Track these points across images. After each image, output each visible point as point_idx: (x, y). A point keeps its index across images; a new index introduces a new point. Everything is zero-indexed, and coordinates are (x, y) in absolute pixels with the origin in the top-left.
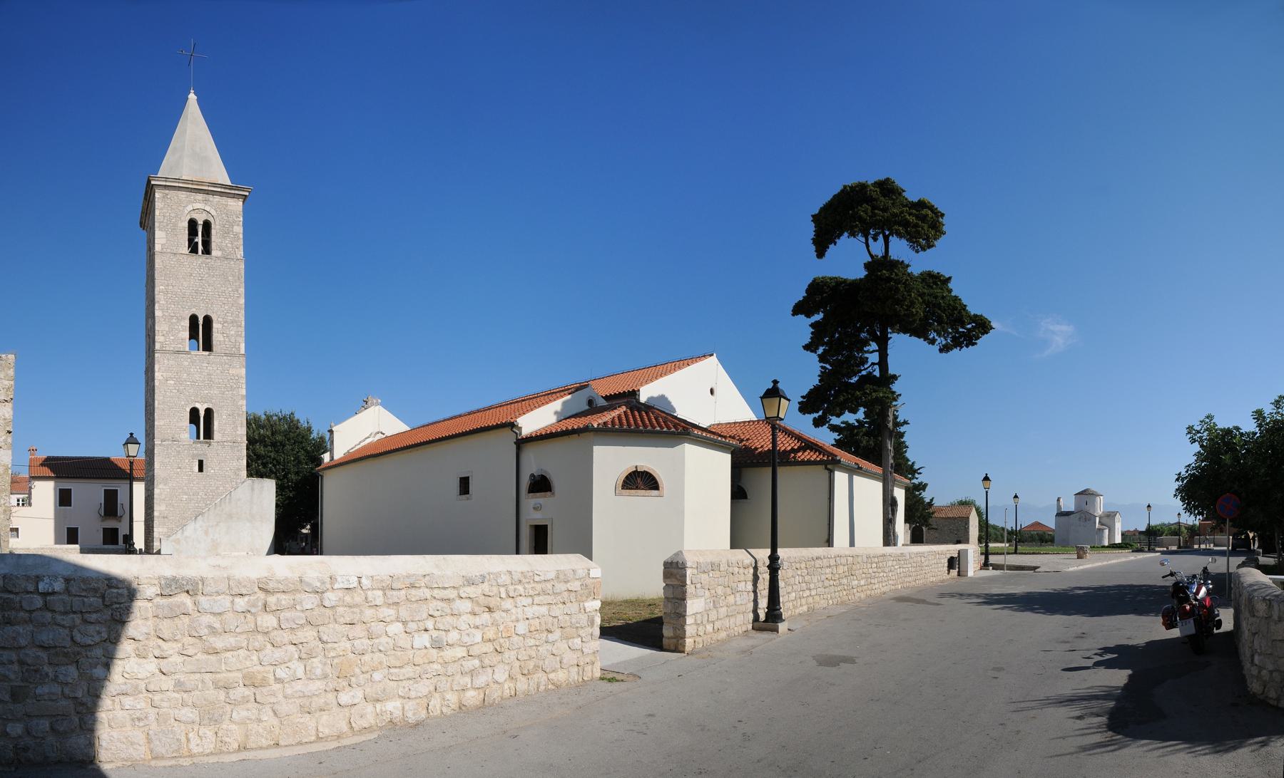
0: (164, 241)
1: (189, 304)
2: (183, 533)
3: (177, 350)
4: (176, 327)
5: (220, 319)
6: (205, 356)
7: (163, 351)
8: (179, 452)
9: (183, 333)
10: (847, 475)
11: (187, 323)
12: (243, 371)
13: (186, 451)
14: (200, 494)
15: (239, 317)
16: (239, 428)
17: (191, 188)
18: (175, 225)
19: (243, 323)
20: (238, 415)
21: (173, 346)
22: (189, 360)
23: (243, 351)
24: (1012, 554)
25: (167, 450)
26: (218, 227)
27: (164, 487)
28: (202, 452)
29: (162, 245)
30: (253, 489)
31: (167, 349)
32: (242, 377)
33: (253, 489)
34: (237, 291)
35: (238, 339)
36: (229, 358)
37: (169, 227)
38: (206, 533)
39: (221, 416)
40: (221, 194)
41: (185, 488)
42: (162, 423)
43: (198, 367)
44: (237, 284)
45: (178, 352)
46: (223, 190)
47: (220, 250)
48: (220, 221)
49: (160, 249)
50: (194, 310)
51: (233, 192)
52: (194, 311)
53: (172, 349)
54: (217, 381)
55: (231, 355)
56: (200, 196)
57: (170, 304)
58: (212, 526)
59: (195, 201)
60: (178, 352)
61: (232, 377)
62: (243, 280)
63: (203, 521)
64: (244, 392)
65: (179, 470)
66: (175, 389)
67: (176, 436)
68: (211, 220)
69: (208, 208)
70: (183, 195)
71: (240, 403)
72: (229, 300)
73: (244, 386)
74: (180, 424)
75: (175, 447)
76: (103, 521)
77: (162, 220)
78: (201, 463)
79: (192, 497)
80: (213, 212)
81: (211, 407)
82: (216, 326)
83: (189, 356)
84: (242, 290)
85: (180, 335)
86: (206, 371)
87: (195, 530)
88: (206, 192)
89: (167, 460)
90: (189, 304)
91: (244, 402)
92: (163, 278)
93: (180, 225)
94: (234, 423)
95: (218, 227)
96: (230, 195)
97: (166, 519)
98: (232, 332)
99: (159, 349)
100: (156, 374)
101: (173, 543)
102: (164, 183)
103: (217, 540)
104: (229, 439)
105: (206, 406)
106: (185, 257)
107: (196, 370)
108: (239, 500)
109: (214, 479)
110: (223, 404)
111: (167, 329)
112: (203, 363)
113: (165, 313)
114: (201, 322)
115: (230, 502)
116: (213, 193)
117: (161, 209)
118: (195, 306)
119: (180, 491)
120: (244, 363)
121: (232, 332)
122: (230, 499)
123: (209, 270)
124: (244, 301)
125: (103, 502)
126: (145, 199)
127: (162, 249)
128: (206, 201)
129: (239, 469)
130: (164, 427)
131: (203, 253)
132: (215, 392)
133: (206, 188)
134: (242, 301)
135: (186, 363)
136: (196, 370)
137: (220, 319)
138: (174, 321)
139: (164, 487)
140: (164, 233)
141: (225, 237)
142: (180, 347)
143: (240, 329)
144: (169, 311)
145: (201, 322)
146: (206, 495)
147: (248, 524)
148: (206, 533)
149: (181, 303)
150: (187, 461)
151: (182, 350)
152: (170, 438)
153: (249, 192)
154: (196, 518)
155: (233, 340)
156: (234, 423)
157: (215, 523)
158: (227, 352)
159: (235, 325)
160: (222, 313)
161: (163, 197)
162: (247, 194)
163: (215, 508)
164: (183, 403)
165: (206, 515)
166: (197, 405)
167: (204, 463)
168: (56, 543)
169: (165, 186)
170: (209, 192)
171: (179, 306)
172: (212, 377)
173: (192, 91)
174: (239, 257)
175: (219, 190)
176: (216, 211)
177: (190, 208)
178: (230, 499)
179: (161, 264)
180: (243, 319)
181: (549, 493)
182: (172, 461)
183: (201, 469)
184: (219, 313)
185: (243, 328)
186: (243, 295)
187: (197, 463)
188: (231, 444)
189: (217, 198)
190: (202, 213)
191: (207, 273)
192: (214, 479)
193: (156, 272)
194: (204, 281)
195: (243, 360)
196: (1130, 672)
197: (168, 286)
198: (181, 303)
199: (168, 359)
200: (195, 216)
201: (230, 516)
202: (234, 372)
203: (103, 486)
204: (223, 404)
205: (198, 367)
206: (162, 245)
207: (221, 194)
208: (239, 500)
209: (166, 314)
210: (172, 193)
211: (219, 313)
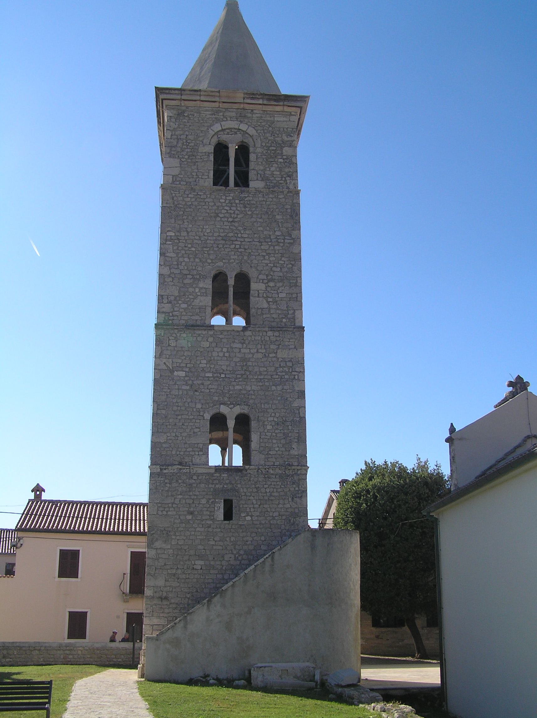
2: (185, 627)
4: (191, 290)
5: (261, 277)
9: (202, 298)
10: (416, 621)
11: (208, 284)
13: (202, 485)
14: (227, 557)
21: (186, 318)
22: (211, 339)
24: (256, 180)
27: (164, 546)
28: (230, 486)
29: (173, 176)
37: (184, 153)
39: (264, 425)
50: (220, 264)
65: (189, 517)
66: (187, 384)
68: (250, 142)
69: (243, 127)
72: (277, 248)
76: (126, 601)
79: (212, 563)
80: (251, 131)
89: (169, 500)
95: (259, 150)
97: (165, 602)
98: (281, 295)
101: (168, 646)
105: (237, 410)
107: (221, 354)
111: (176, 294)
112: (234, 342)
113: (173, 270)
114: (231, 282)
121: (281, 295)
123: (245, 207)
125: (128, 571)
126: (159, 123)
131: (236, 185)
132: (254, 387)
135: (206, 344)
137: (261, 277)
139: (164, 546)
145: (231, 282)
150: (204, 501)
158: (274, 324)
164: (199, 406)
166: (224, 409)
168: (69, 637)
172: (250, 363)
176: (257, 131)
177: (217, 127)
181: (140, 596)
182: (177, 501)
183: (228, 515)
184: (260, 268)
190: (236, 133)
191: (241, 212)
200: (224, 138)
202: (285, 356)
203: (128, 547)
204: (267, 406)
205: (225, 350)
206: (173, 176)
211: (260, 268)
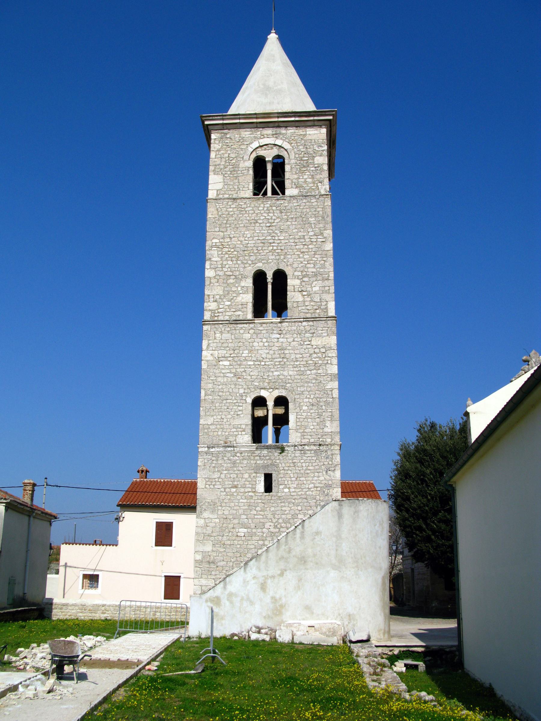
0: (220, 186)
1: (253, 258)
2: (225, 587)
3: (234, 318)
5: (296, 273)
6: (276, 323)
7: (214, 322)
8: (234, 463)
9: (244, 296)
11: (249, 283)
12: (333, 340)
14: (267, 525)
15: (325, 268)
16: (328, 424)
17: (257, 123)
18: (235, 167)
19: (332, 275)
20: (327, 403)
21: (229, 314)
23: (332, 312)
25: (217, 460)
26: (293, 161)
27: (211, 516)
29: (217, 190)
30: (340, 516)
31: (221, 318)
32: (330, 348)
33: (340, 516)
34: (322, 234)
35: (325, 296)
36: (311, 323)
37: (227, 169)
38: (263, 587)
40: (297, 124)
41: (244, 517)
42: (210, 421)
43: (264, 340)
44: (321, 225)
45: (236, 322)
46: (297, 119)
47: (297, 187)
48: (295, 154)
49: (215, 195)
51: (312, 118)
52: (260, 266)
53: (227, 318)
54: (293, 356)
55: (314, 319)
56: (269, 131)
57: (227, 260)
58: (273, 577)
59: (263, 136)
60: (236, 322)
61: (317, 350)
62: (329, 219)
63: (259, 569)
64: (334, 369)
65: (234, 490)
66: (231, 372)
67: (231, 439)
68: (284, 154)
69: (279, 142)
70: (246, 133)
71: (329, 387)
73: (335, 361)
74: (237, 422)
75: (228, 455)
77: (218, 162)
78: (268, 478)
80: (286, 145)
81: (284, 394)
82: (291, 282)
83: (252, 325)
84: (329, 233)
85: (239, 299)
86: (276, 344)
87: (245, 582)
88: (277, 124)
89: (216, 475)
90: (253, 258)
91: (335, 384)
92: (217, 229)
93: (242, 165)
94: (320, 415)
96: (309, 123)
97: (212, 565)
99: (209, 319)
100: (204, 353)
102: (221, 122)
103: (280, 599)
104: (312, 440)
105: (277, 393)
106: (248, 201)
108: (318, 533)
109: (289, 503)
110: (302, 389)
111: (221, 293)
115: (302, 537)
116: (285, 124)
117: (219, 150)
118: (260, 261)
119: (236, 521)
120: (334, 329)
121: (314, 289)
122: (302, 533)
123: (281, 212)
124: (331, 245)
127: (218, 195)
128: (276, 136)
129: (329, 486)
130: (212, 427)
132: (291, 373)
133: (276, 120)
134: (329, 246)
135: (247, 336)
136: (261, 344)
137: (296, 273)
138: (231, 281)
140: (221, 177)
141: (303, 172)
142: (240, 315)
143: (327, 283)
144: (225, 270)
146: (275, 527)
147: (333, 574)
148: (263, 587)
149: (241, 258)
150: (246, 476)
151: (241, 318)
152: (222, 442)
153: (333, 115)
154: (246, 564)
155: (317, 298)
156: (320, 415)
157: (279, 572)
158: (309, 315)
159: (319, 278)
160: (300, 266)
161: (221, 138)
162: (331, 118)
163: (278, 548)
164: (242, 391)
165: (263, 558)
166: (264, 393)
167: (274, 478)
169: (223, 124)
170: (281, 124)
171: (239, 262)
173: (273, 31)
174: (323, 192)
175: (293, 119)
177: (256, 144)
178: (302, 533)
179: (216, 212)
180: (331, 269)
182: (223, 476)
183: (268, 488)
184: (295, 265)
185: (333, 282)
186: (331, 239)
187: (263, 479)
188: (315, 448)
189: (291, 131)
190: (272, 148)
192: (289, 503)
193: (208, 223)
194: (274, 228)
195: (332, 324)
196: (273, 37)
197: (223, 238)
198: (241, 258)
199: (221, 333)
200: (261, 152)
201: (303, 560)
202: (319, 343)
204: (302, 389)
206: (217, 190)
207: (297, 125)
208: (318, 533)
209: (221, 273)
210: (233, 134)
211: (295, 265)
